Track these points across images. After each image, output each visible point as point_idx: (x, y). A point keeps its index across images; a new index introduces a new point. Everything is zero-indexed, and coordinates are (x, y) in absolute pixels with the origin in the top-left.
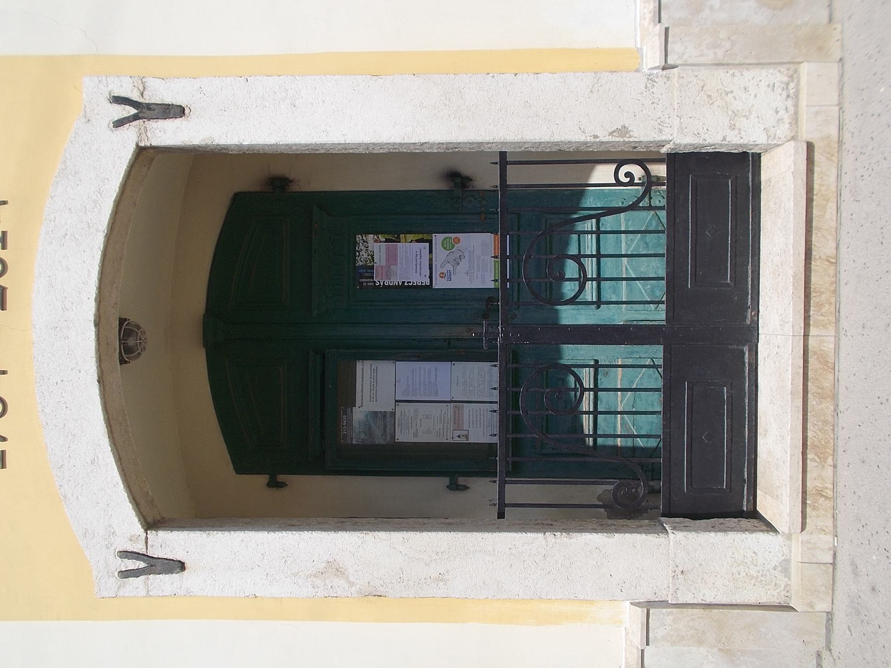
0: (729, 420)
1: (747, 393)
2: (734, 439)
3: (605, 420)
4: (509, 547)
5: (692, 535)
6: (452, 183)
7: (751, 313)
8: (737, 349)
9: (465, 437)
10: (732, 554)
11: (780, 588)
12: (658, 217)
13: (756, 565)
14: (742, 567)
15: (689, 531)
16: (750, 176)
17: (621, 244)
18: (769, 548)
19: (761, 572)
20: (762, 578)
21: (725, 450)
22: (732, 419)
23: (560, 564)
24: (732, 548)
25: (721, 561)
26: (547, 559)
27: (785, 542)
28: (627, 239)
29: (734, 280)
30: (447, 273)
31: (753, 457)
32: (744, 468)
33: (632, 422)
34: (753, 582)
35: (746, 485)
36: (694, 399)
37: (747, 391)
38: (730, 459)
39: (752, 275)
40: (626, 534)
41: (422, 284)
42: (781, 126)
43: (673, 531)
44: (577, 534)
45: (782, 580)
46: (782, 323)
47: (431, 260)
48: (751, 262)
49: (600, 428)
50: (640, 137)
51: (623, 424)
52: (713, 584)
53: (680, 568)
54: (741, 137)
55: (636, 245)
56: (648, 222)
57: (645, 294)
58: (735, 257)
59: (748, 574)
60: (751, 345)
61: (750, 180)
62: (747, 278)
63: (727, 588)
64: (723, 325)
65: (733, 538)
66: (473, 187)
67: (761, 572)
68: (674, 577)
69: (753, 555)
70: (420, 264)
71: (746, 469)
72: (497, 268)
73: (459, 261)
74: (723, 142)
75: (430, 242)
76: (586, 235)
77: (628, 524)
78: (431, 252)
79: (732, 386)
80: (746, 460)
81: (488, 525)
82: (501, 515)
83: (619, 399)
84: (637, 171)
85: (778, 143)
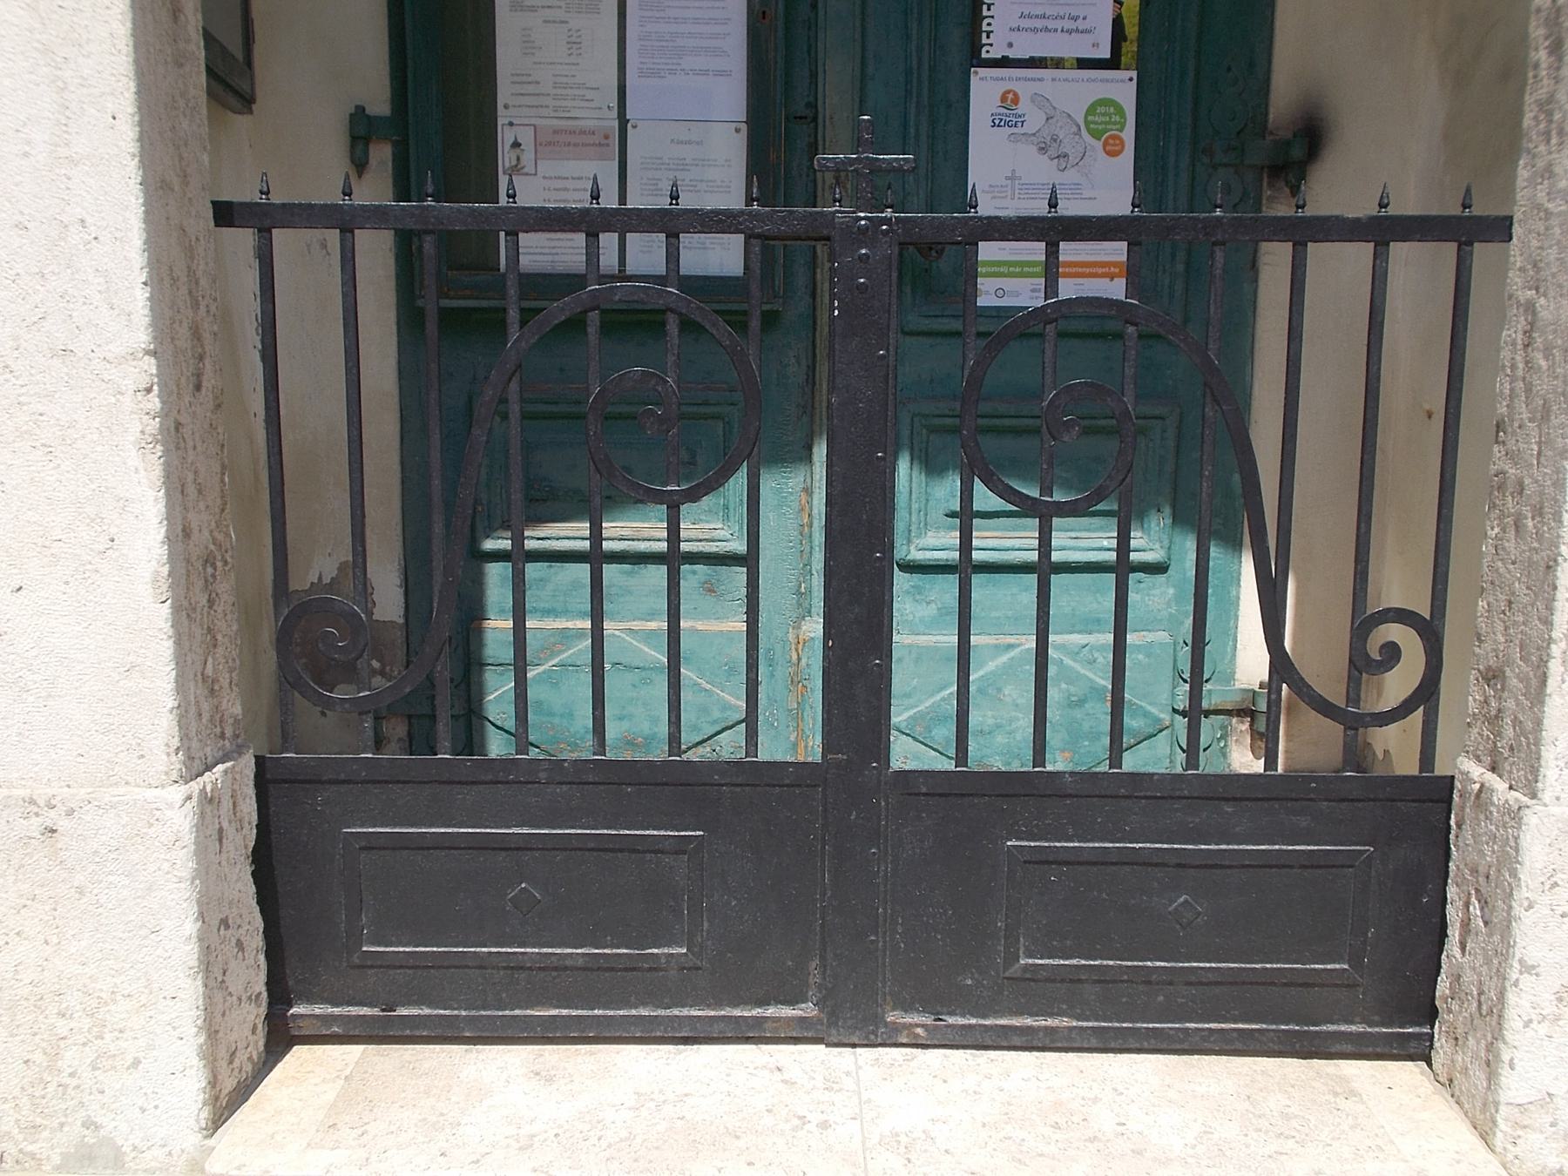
0: (580, 962)
1: (668, 1012)
2: (523, 975)
3: (575, 585)
4: (89, 220)
5: (184, 861)
6: (1290, 135)
7: (922, 1026)
8: (808, 986)
9: (514, 163)
10: (126, 992)
11: (25, 1140)
12: (1155, 735)
13: (95, 1069)
14: (86, 1023)
15: (201, 851)
16: (1353, 1028)
17: (1080, 632)
18: (156, 1107)
19: (74, 1082)
20: (51, 1088)
21: (485, 950)
22: (584, 969)
23: (41, 409)
24: (146, 991)
25: (99, 955)
26: (56, 362)
27: (179, 1157)
28: (1094, 648)
29: (1028, 976)
30: (1016, 116)
31: (468, 1034)
32: (429, 1006)
33: (570, 662)
34: (38, 1057)
35: (376, 1011)
36: (648, 856)
37: (676, 1012)
38: (460, 962)
39: (1039, 1028)
40: (170, 643)
41: (984, 35)
42: (1554, 1145)
43: (195, 799)
44: (157, 471)
45: (52, 1148)
46: (903, 1139)
47: (1058, 63)
48: (1082, 1028)
49: (552, 570)
50: (1563, 696)
51: (566, 636)
52: (18, 934)
53: (63, 824)
54: (1531, 1021)
55: (1078, 672)
56: (1141, 707)
57: (938, 697)
58: (1099, 982)
59: (62, 1043)
60: (822, 1024)
61: (1343, 1028)
62: (1031, 1015)
63: (9, 976)
64: (884, 946)
65: (181, 995)
66: (1271, 199)
67: (74, 1082)
68: (32, 802)
69: (129, 1060)
70: (1047, 30)
71: (427, 1011)
72: (1026, 269)
73: (1052, 152)
74: (1516, 965)
75: (1113, 63)
76: (1116, 534)
77: (220, 650)
78: (1083, 64)
79: (689, 969)
80: (456, 1012)
81: (181, 158)
82: (225, 214)
83: (636, 625)
84: (1397, 685)
85: (1499, 1135)
